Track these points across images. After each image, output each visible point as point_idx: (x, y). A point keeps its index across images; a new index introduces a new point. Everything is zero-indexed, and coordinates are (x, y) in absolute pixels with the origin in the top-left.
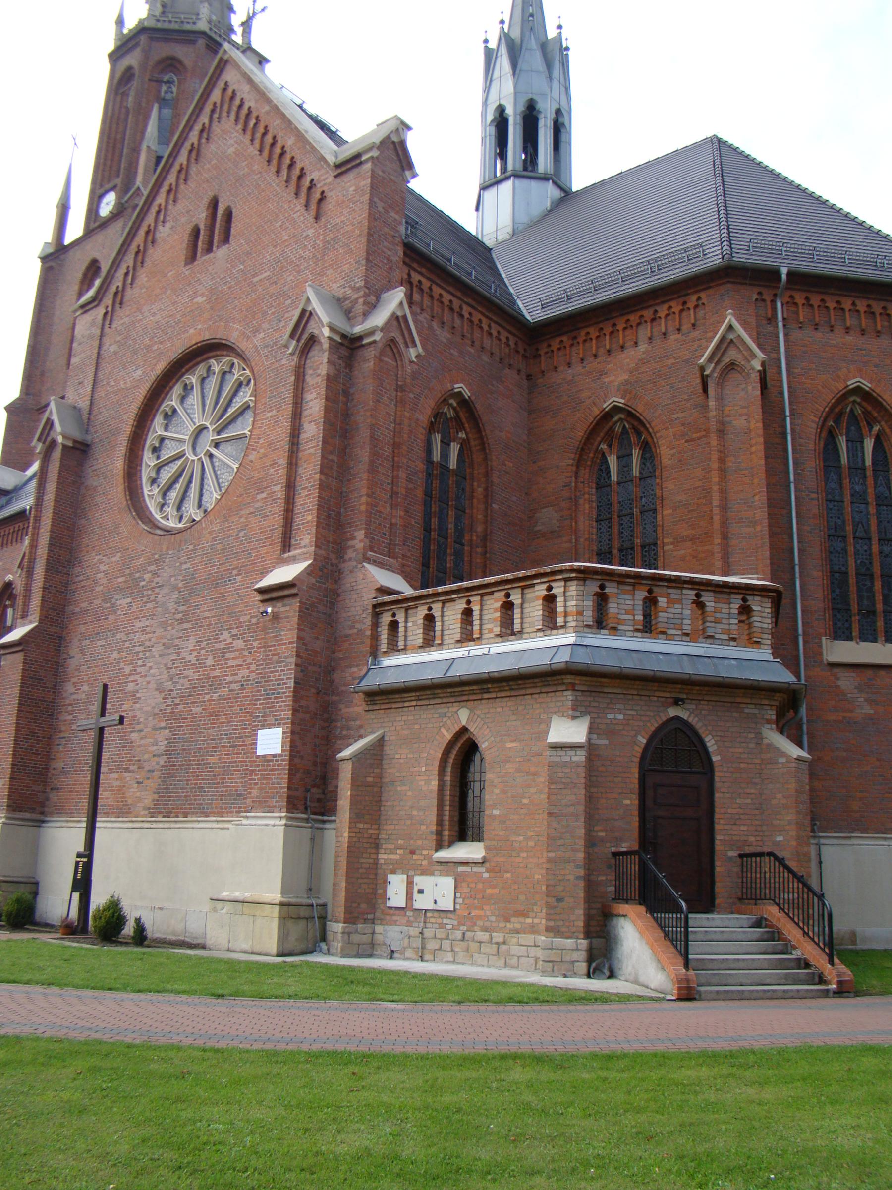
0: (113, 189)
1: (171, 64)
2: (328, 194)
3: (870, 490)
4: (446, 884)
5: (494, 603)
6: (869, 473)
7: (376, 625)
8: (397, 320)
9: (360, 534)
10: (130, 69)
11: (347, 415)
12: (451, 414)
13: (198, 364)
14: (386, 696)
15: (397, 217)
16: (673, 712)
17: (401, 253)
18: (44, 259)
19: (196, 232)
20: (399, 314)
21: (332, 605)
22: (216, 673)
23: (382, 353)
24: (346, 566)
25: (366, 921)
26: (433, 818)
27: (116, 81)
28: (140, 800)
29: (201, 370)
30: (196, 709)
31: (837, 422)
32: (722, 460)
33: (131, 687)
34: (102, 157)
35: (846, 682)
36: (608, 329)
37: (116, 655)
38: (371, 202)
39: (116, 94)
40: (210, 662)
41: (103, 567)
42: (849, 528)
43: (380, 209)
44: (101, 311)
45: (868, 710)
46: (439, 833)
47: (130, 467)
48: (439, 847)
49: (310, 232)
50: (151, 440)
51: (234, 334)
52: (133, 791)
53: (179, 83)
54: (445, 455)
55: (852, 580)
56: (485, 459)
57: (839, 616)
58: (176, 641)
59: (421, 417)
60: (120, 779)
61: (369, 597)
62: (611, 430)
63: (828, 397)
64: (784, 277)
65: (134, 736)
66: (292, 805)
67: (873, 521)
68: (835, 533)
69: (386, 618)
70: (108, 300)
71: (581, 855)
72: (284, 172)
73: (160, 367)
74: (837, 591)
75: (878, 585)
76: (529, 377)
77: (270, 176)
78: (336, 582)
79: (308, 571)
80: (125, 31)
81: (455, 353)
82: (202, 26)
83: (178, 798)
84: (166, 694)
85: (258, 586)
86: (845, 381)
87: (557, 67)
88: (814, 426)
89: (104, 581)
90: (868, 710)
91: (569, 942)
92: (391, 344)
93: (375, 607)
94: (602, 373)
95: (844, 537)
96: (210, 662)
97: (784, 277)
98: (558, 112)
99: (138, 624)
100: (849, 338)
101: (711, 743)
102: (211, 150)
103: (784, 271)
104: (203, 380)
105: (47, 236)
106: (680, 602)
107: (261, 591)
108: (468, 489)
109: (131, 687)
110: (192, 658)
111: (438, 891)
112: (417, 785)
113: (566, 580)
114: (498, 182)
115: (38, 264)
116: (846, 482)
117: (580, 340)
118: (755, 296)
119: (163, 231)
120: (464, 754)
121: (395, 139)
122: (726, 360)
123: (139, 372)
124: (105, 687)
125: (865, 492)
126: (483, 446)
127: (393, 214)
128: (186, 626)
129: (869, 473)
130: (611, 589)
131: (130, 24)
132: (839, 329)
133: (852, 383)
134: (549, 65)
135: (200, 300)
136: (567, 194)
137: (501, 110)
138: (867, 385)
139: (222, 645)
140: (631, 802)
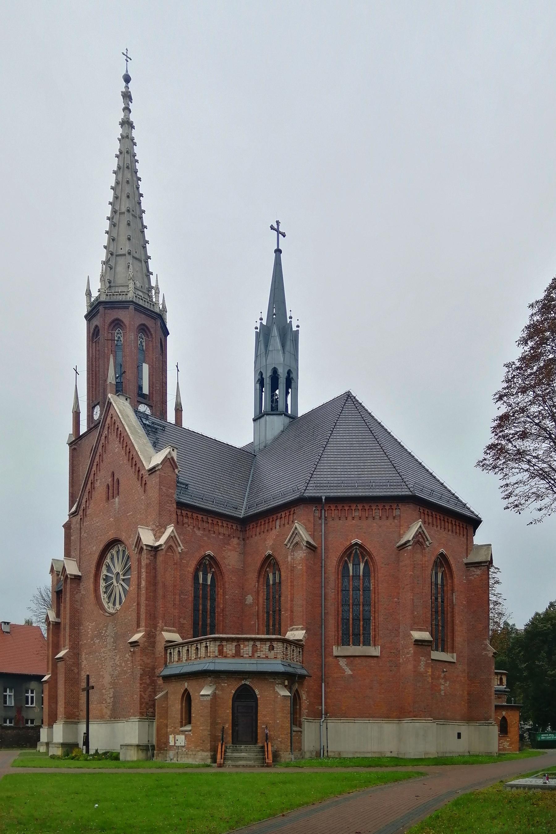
0: (98, 404)
1: (117, 323)
2: (147, 482)
3: (361, 586)
4: (183, 737)
5: (194, 648)
6: (361, 578)
7: (166, 653)
8: (170, 537)
9: (160, 621)
10: (97, 326)
11: (155, 577)
12: (207, 562)
13: (115, 546)
14: (167, 678)
15: (172, 491)
16: (243, 682)
17: (175, 506)
18: (70, 444)
19: (108, 486)
20: (172, 535)
21: (154, 647)
22: (125, 669)
23: (167, 551)
24: (157, 633)
25: (164, 750)
26: (180, 717)
27: (92, 331)
28: (106, 713)
29: (109, 556)
30: (121, 682)
31: (349, 557)
32: (292, 582)
33: (101, 673)
34: (91, 383)
35: (342, 663)
36: (267, 521)
37: (96, 661)
38: (160, 489)
39: (93, 343)
40: (123, 665)
41: (90, 627)
42: (351, 601)
43: (164, 490)
44: (79, 517)
45: (350, 673)
46: (181, 722)
47: (95, 587)
48: (182, 726)
49: (143, 497)
50: (102, 576)
51: (123, 538)
52: (105, 710)
53: (124, 335)
54: (205, 579)
55: (351, 622)
56: (223, 578)
57: (345, 636)
58: (114, 657)
59: (190, 570)
60: (101, 706)
61: (163, 644)
62: (270, 562)
63: (342, 549)
64: (323, 500)
65: (104, 691)
66: (141, 714)
67: (362, 597)
68: (345, 603)
69: (169, 651)
70: (81, 513)
71: (209, 728)
72: (134, 467)
73: (101, 547)
74: (345, 627)
75: (362, 623)
76: (244, 539)
77: (130, 468)
78: (155, 638)
79: (143, 637)
80: (92, 299)
81: (205, 538)
82: (130, 296)
83: (116, 715)
84: (112, 676)
85: (130, 641)
86: (350, 541)
87: (289, 344)
88: (335, 562)
89: (90, 633)
90: (350, 673)
91: (206, 754)
92: (170, 547)
93: (165, 647)
94: (265, 540)
95: (349, 605)
96: (123, 665)
97: (323, 500)
98: (289, 372)
99: (102, 650)
100: (354, 521)
101: (257, 692)
102: (109, 447)
103: (324, 498)
104: (118, 552)
105: (69, 429)
106: (248, 646)
107: (131, 643)
108: (216, 591)
109: (101, 673)
110: (118, 663)
111: (181, 740)
112: (176, 707)
113: (210, 641)
114: (260, 418)
115: (68, 447)
116: (351, 582)
117: (259, 525)
118: (314, 509)
119: (97, 484)
120: (187, 698)
121: (169, 457)
122: (295, 542)
123: (95, 548)
124: (88, 676)
125: (359, 586)
126: (221, 573)
127: (170, 491)
128: (117, 651)
129: (361, 578)
130: (224, 643)
131: (95, 294)
132: (350, 518)
133: (353, 542)
134: (283, 346)
135: (112, 519)
136: (293, 418)
137: (275, 371)
138: (360, 542)
139: (126, 659)
140: (229, 711)
